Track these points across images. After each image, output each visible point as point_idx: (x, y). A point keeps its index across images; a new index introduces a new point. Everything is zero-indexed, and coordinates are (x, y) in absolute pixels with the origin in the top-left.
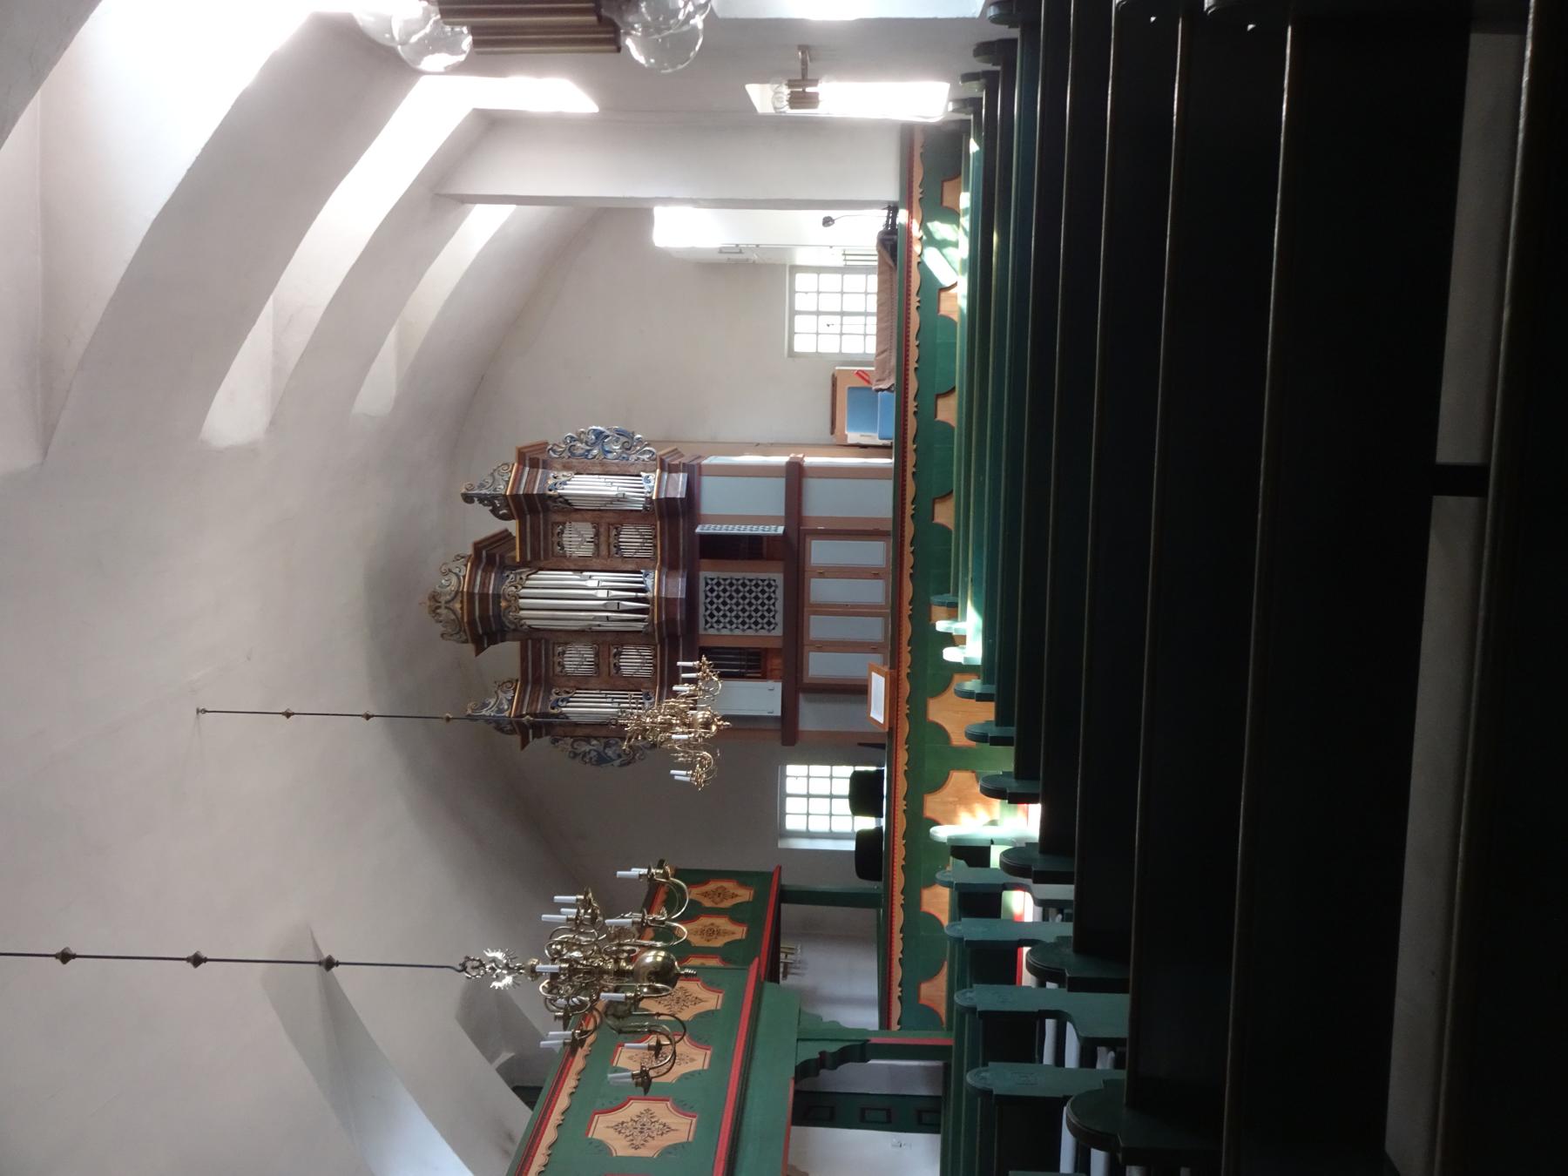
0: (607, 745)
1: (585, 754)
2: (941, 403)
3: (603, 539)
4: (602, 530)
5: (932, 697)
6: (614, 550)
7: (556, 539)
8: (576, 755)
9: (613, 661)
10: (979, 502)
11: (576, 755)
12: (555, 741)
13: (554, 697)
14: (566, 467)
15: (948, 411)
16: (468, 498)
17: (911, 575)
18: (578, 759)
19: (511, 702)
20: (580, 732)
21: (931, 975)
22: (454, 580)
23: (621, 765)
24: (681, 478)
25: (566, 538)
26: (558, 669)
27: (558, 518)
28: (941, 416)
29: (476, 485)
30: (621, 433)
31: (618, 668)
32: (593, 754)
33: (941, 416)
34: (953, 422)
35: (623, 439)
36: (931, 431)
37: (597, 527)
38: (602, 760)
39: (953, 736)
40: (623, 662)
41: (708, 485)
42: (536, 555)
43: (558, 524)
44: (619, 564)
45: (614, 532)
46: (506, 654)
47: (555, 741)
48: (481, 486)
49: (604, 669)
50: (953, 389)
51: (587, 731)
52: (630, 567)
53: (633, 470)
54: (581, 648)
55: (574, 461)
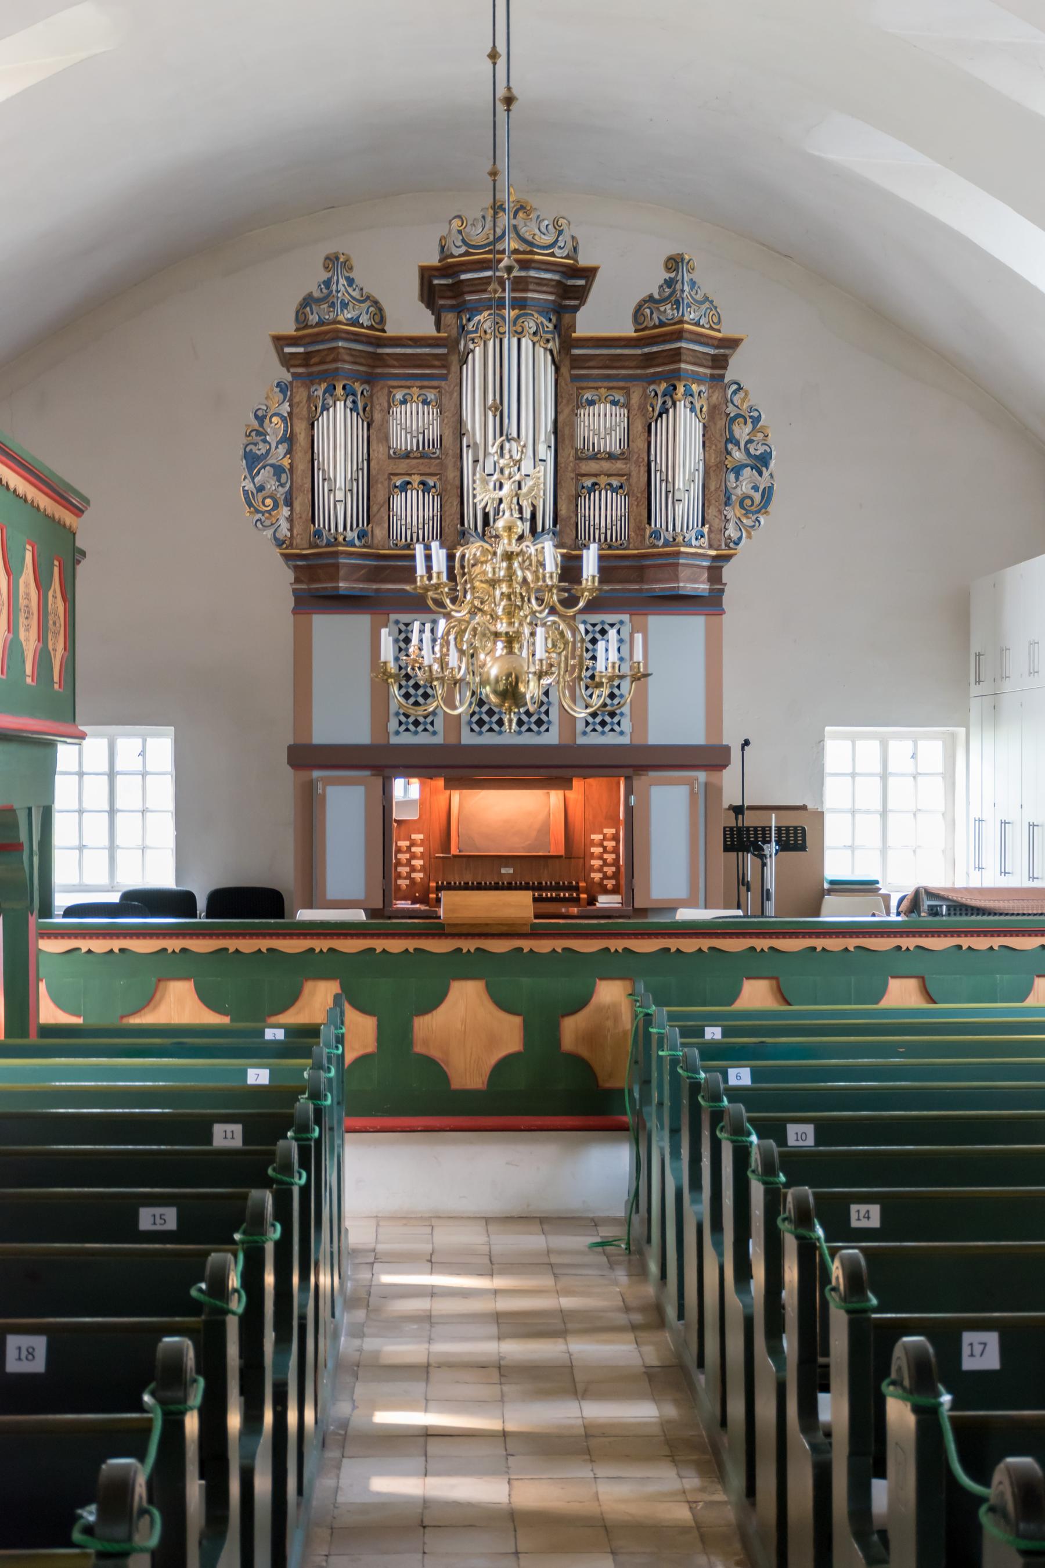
0: (278, 470)
1: (262, 434)
2: (912, 984)
3: (606, 465)
4: (619, 465)
5: (488, 988)
6: (588, 482)
7: (415, 391)
8: (261, 419)
9: (416, 480)
10: (913, 1050)
11: (261, 419)
12: (282, 387)
13: (358, 387)
14: (714, 410)
15: (902, 994)
16: (674, 263)
17: (753, 949)
18: (255, 424)
19: (697, 324)
20: (300, 428)
21: (208, 998)
22: (548, 239)
23: (246, 492)
24: (702, 587)
25: (604, 408)
26: (399, 396)
27: (635, 399)
28: (894, 984)
29: (694, 276)
30: (767, 495)
31: (405, 487)
32: (262, 449)
33: (894, 984)
34: (885, 1003)
35: (757, 497)
36: (879, 969)
37: (623, 457)
38: (253, 461)
39: (427, 1018)
40: (413, 496)
41: (691, 627)
42: (577, 362)
43: (628, 395)
44: (568, 488)
45: (615, 483)
46: (410, 319)
47: (282, 387)
48: (693, 284)
49: (403, 466)
50: (790, 1004)
51: (302, 439)
52: (563, 511)
53: (712, 512)
54: (619, 433)
55: (721, 423)
